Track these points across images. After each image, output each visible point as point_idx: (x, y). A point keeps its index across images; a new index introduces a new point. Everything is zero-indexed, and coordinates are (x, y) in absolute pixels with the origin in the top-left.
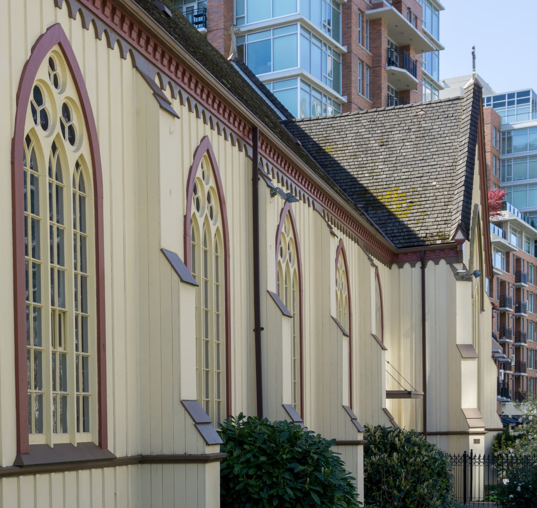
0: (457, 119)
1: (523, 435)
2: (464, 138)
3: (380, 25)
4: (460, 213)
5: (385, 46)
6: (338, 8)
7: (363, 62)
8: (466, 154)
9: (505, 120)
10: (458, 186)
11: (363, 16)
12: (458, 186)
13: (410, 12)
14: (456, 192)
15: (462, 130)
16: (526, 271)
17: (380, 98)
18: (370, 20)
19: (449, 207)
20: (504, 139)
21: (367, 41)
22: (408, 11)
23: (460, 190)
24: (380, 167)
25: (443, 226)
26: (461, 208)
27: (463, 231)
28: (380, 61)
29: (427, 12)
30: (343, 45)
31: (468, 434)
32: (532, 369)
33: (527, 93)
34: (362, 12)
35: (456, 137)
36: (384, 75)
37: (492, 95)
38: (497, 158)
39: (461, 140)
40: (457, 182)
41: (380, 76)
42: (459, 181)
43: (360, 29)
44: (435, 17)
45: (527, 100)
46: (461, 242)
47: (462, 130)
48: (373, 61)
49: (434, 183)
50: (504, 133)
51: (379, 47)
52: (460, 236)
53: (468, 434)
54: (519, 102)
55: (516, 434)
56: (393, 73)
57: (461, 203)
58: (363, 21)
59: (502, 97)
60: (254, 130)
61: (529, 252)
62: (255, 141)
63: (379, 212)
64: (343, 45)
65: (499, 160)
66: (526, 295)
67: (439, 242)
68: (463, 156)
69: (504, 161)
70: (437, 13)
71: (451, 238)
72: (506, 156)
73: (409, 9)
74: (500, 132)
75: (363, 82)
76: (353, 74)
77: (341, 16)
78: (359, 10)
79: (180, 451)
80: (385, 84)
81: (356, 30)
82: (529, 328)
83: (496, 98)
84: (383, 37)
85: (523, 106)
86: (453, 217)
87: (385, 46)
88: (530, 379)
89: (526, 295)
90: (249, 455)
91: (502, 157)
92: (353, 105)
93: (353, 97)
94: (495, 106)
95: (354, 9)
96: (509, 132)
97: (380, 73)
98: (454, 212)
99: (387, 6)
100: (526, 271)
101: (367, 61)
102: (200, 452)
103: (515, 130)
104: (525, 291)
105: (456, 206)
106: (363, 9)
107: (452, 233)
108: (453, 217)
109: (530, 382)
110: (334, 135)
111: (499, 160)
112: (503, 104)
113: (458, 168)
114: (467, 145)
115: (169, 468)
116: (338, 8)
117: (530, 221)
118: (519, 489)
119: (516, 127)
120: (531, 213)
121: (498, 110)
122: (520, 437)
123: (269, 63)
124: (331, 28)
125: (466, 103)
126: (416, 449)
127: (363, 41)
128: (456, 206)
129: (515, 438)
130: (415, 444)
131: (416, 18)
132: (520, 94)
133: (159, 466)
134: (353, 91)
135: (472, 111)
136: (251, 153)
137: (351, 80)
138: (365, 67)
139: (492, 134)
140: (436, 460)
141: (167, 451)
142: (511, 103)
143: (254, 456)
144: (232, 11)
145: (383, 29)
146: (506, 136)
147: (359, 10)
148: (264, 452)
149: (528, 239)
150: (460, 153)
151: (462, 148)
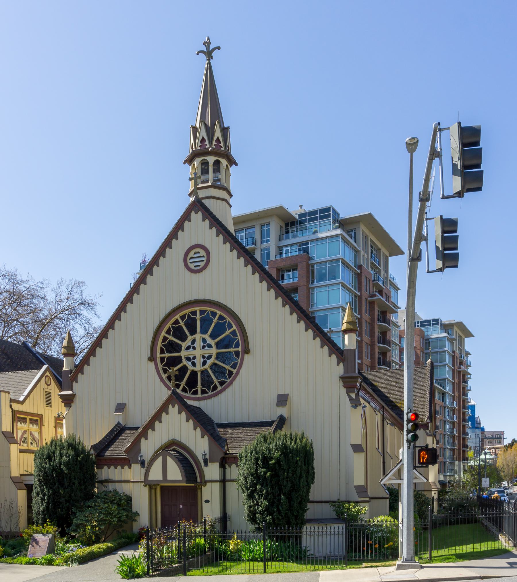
0: (425, 375)
1: (452, 491)
2: (428, 383)
3: (374, 304)
4: (428, 412)
5: (376, 313)
6: (356, 298)
7: (367, 321)
8: (429, 390)
9: (426, 333)
10: (427, 402)
11: (367, 301)
12: (427, 402)
13: (386, 295)
14: (426, 404)
15: (427, 380)
16: (438, 410)
17: (375, 337)
18: (370, 302)
19: (424, 409)
20: (426, 343)
21: (369, 311)
22: (385, 294)
23: (427, 403)
24: (396, 392)
25: (422, 416)
26: (428, 410)
27: (429, 419)
28: (374, 320)
29: (393, 292)
30: (358, 315)
31: (432, 491)
32: (441, 457)
33: (437, 320)
34: (366, 299)
35: (424, 382)
36: (376, 326)
37: (420, 321)
38: (423, 352)
39: (427, 383)
40: (426, 400)
41: (375, 327)
42: (427, 400)
43: (366, 307)
44: (396, 294)
45: (438, 324)
46: (429, 423)
47: (427, 380)
48: (371, 320)
49: (417, 400)
50: (426, 340)
51: (374, 314)
52: (428, 421)
53: (432, 491)
54: (433, 324)
55: (449, 491)
56: (380, 325)
57: (428, 409)
58: (367, 303)
59: (425, 321)
60: (383, 407)
61: (439, 400)
62: (383, 410)
63: (397, 410)
64: (358, 315)
65: (424, 353)
66: (438, 421)
67: (421, 422)
68: (428, 390)
69: (426, 354)
70: (397, 291)
71: (425, 421)
72: (427, 351)
73: (386, 293)
74: (424, 339)
75: (367, 330)
76: (363, 327)
77: (357, 301)
78: (365, 298)
79: (381, 496)
80: (377, 330)
81: (364, 307)
82: (440, 436)
83: (422, 322)
84: (376, 309)
85: (435, 326)
86: (426, 413)
87: (376, 313)
88: (440, 462)
89: (438, 421)
90: (393, 497)
91: (425, 352)
92: (363, 341)
93: (363, 338)
94: (421, 326)
95: (363, 298)
96: (428, 339)
97: (375, 326)
98: (426, 412)
99: (378, 296)
100: (438, 410)
101: (369, 321)
102: (386, 496)
103: (431, 338)
104: (438, 419)
105: (426, 409)
106: (367, 298)
107: (426, 419)
108: (426, 413)
109: (440, 464)
110: (378, 379)
111: (424, 353)
112: (425, 325)
113: (427, 394)
114: (429, 386)
115: (378, 500)
116: (356, 298)
117: (440, 384)
118: (452, 509)
119: (432, 337)
120: (440, 380)
121: (423, 328)
122: (450, 492)
123: (327, 325)
124: (353, 308)
125: (428, 369)
126: (421, 496)
127: (367, 312)
128: (426, 409)
129: (449, 492)
130: (420, 494)
131: (389, 297)
132: (434, 320)
133: (375, 500)
134: (363, 335)
135: (430, 372)
136: (382, 413)
137: (362, 330)
138: (368, 323)
139: (420, 341)
140: (426, 499)
141: (377, 496)
142: (429, 325)
143: (394, 497)
144: (309, 301)
145: (376, 306)
146: (427, 341)
147: (365, 298)
148: (85, 511)
149: (439, 393)
150: (427, 389)
151: (427, 387)
